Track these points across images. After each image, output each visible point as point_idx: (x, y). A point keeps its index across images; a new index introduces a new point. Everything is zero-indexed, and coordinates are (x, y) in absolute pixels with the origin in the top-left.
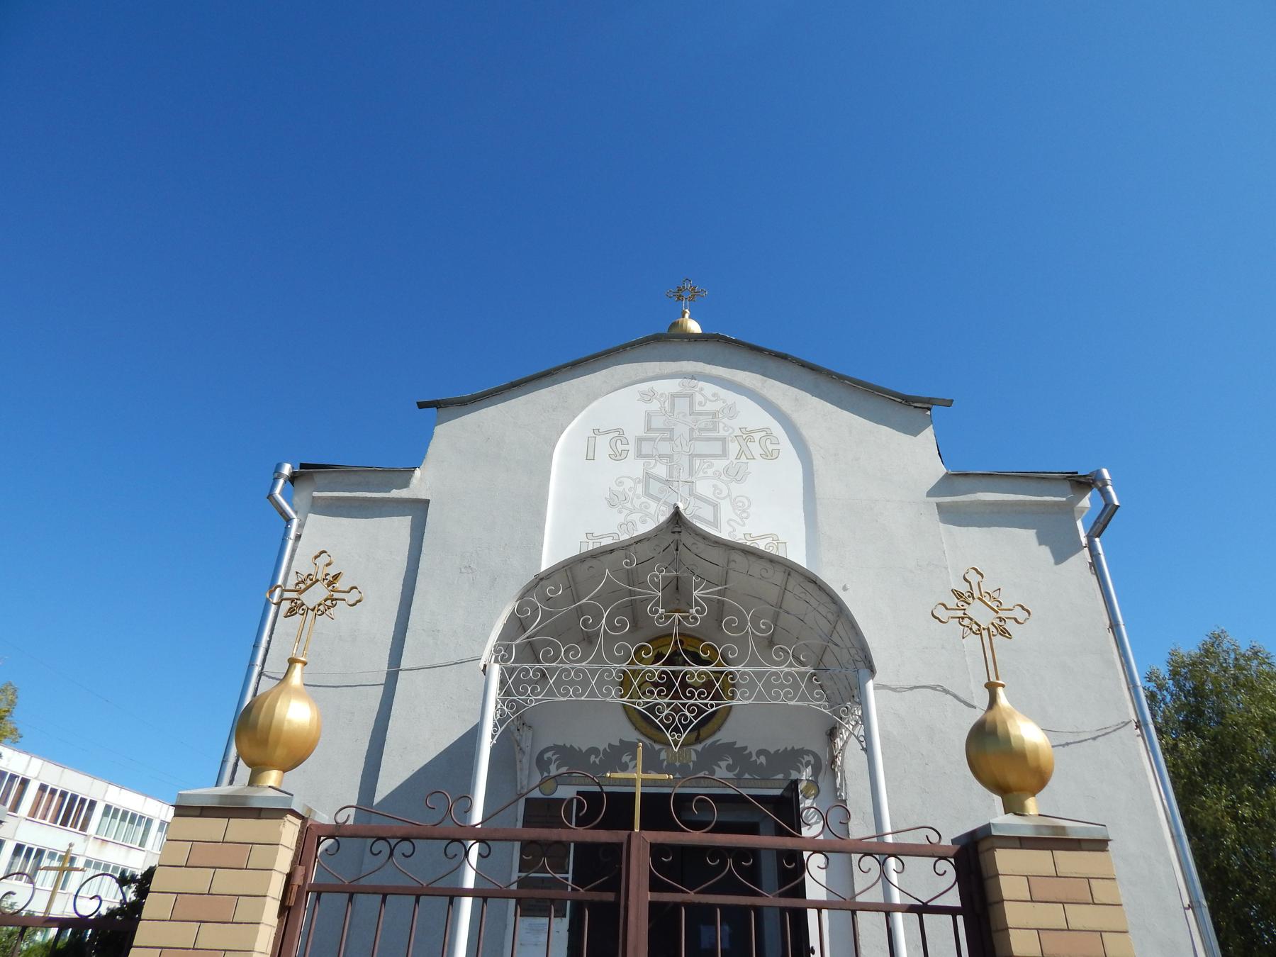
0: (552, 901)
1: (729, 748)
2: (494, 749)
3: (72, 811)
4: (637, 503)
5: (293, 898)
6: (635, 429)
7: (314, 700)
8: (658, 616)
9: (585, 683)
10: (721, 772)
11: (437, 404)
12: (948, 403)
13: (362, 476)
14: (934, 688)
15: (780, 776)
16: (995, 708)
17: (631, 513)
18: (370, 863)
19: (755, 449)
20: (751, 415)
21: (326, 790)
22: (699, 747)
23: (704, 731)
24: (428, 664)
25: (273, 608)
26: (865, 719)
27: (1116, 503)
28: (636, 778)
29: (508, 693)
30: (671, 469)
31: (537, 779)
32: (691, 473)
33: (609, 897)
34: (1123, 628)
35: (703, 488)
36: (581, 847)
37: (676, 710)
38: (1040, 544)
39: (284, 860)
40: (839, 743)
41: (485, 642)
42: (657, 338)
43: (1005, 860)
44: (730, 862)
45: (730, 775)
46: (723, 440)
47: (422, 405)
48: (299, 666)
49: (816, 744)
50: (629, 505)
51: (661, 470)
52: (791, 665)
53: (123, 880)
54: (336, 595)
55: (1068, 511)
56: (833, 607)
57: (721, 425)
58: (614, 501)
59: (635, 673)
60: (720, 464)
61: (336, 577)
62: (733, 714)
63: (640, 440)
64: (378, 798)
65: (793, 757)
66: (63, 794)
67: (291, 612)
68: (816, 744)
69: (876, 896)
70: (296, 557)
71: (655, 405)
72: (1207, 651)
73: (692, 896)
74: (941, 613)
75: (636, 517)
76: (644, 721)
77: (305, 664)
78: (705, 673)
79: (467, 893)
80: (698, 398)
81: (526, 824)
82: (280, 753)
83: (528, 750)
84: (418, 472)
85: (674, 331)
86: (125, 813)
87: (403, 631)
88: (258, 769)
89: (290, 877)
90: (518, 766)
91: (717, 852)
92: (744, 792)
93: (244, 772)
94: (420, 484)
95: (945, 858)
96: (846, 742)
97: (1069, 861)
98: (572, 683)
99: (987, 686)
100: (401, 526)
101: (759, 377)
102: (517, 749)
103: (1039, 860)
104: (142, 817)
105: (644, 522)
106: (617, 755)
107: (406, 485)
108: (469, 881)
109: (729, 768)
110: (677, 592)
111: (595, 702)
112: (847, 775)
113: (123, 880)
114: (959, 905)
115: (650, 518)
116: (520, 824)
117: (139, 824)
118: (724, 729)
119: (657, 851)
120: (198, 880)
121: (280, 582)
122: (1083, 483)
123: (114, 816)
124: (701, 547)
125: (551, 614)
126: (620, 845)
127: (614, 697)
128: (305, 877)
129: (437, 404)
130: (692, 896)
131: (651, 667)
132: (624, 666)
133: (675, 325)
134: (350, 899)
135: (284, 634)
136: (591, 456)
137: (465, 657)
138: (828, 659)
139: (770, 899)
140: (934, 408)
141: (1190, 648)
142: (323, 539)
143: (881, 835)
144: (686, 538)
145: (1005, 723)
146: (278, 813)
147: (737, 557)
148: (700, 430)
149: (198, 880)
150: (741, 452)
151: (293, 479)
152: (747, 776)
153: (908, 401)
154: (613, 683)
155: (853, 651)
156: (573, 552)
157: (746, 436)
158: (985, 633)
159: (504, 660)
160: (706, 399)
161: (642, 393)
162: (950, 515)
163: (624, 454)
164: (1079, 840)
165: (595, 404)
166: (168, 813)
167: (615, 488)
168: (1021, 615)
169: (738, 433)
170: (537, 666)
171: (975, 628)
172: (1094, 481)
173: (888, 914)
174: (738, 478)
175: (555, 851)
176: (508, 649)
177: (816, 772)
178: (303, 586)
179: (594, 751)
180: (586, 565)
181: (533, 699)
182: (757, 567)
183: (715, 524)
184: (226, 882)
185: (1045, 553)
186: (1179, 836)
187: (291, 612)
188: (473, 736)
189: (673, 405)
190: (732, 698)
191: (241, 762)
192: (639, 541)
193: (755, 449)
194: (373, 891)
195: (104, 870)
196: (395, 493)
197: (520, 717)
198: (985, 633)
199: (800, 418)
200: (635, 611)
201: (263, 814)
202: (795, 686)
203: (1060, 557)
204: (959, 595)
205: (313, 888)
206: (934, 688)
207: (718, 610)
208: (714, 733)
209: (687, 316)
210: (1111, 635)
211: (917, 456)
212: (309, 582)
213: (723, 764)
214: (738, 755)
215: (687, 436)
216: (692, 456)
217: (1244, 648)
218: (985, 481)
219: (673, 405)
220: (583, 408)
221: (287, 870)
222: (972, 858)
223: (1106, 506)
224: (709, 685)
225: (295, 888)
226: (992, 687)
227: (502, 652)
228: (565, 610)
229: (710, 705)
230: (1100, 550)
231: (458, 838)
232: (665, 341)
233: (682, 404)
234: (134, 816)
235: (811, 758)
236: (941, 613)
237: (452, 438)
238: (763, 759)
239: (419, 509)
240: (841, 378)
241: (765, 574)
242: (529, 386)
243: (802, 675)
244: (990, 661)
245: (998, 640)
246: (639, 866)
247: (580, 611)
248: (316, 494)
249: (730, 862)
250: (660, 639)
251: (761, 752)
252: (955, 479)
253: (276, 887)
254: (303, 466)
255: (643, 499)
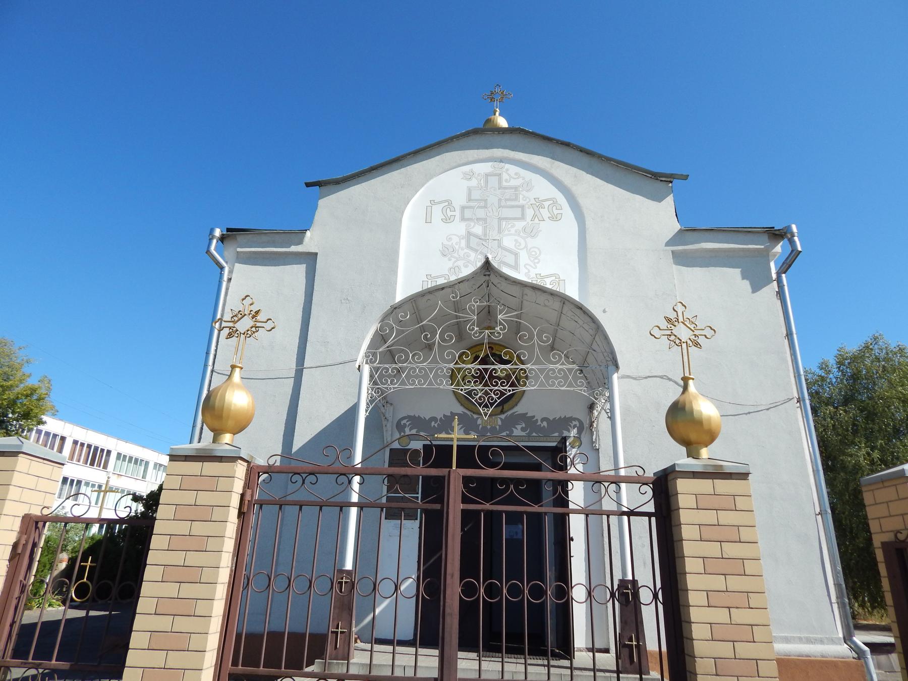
0: (403, 509)
1: (523, 417)
2: (367, 419)
3: (96, 457)
4: (461, 253)
5: (246, 507)
6: (460, 200)
7: (248, 389)
8: (475, 332)
9: (426, 377)
10: (517, 432)
11: (319, 184)
12: (685, 177)
13: (270, 237)
14: (661, 377)
15: (556, 434)
16: (687, 393)
17: (457, 260)
18: (291, 487)
19: (545, 213)
20: (543, 189)
21: (262, 445)
22: (503, 416)
23: (506, 406)
24: (323, 364)
25: (216, 332)
26: (610, 399)
27: (800, 249)
28: (456, 436)
29: (375, 383)
30: (485, 229)
31: (397, 435)
32: (500, 231)
33: (437, 506)
34: (795, 336)
35: (508, 242)
36: (426, 479)
37: (486, 393)
38: (743, 279)
39: (238, 486)
40: (596, 413)
41: (359, 349)
42: (476, 132)
43: (682, 485)
44: (512, 486)
45: (524, 434)
46: (522, 207)
47: (308, 185)
48: (238, 370)
49: (582, 415)
50: (456, 255)
51: (478, 230)
52: (563, 364)
53: (136, 498)
54: (258, 324)
55: (765, 256)
56: (593, 325)
57: (521, 196)
58: (447, 251)
59: (459, 370)
60: (520, 225)
61: (257, 312)
62: (526, 395)
63: (463, 208)
64: (295, 448)
65: (565, 422)
66: (89, 446)
67: (230, 336)
68: (582, 415)
69: (613, 507)
70: (229, 293)
71: (474, 182)
72: (867, 347)
73: (488, 506)
74: (656, 332)
75: (460, 263)
76: (465, 400)
77: (242, 368)
78: (505, 369)
79: (354, 505)
80: (505, 176)
81: (391, 464)
82: (230, 423)
83: (390, 419)
84: (308, 233)
85: (488, 126)
86: (131, 458)
87: (302, 342)
88: (217, 433)
89: (243, 496)
90: (385, 429)
91: (505, 481)
92: (520, 444)
93: (208, 435)
94: (311, 242)
95: (646, 484)
96: (600, 413)
97: (722, 485)
98: (417, 377)
99: (682, 379)
100: (299, 271)
101: (549, 160)
102: (383, 418)
103: (705, 485)
104: (142, 461)
105: (466, 266)
106: (446, 424)
107: (300, 242)
108: (355, 498)
109: (523, 429)
110: (488, 316)
111: (434, 390)
112: (600, 433)
113: (136, 498)
114: (653, 511)
115: (469, 266)
116: (386, 465)
117: (140, 465)
118: (520, 405)
119: (466, 480)
120: (188, 497)
121: (219, 316)
122: (777, 235)
123: (124, 460)
124: (504, 285)
125: (403, 332)
126: (444, 477)
127: (446, 385)
128: (252, 496)
129: (319, 184)
130: (488, 506)
131: (469, 366)
132: (452, 365)
133: (488, 121)
134: (280, 508)
135: (225, 350)
136: (429, 220)
137: (347, 359)
138: (590, 359)
139: (547, 508)
140: (675, 181)
141: (853, 347)
142: (248, 284)
143: (617, 469)
144: (493, 278)
145: (691, 402)
146: (233, 459)
147: (528, 291)
148: (506, 200)
149: (188, 497)
150: (535, 216)
151: (222, 239)
152: (534, 434)
153: (656, 176)
154: (444, 376)
155: (605, 354)
156: (417, 289)
157: (539, 204)
158: (684, 345)
159: (372, 362)
160: (511, 177)
161: (465, 174)
162: (681, 259)
163: (452, 219)
164: (731, 473)
165: (431, 182)
166: (165, 460)
167: (446, 243)
168: (708, 333)
169: (533, 202)
170: (394, 366)
171: (678, 341)
172: (785, 233)
173: (587, 515)
174: (532, 234)
175: (408, 483)
176: (374, 354)
177: (580, 431)
178: (236, 319)
179: (434, 419)
180: (426, 298)
181: (392, 387)
182: (542, 298)
183: (516, 267)
184: (205, 498)
185: (746, 285)
186: (818, 470)
187: (230, 336)
188: (353, 411)
189: (487, 182)
190: (525, 385)
191: (205, 427)
192: (461, 281)
193: (545, 213)
194: (294, 503)
195: (125, 493)
196: (293, 249)
197: (385, 398)
198: (684, 345)
199: (577, 190)
200: (460, 331)
201: (733, 476)
202: (565, 377)
203: (755, 288)
204: (669, 320)
205: (257, 502)
206: (661, 377)
207: (516, 328)
208: (513, 407)
209: (497, 114)
210: (786, 341)
211: (660, 216)
212: (240, 316)
213: (519, 427)
214: (529, 421)
215: (497, 205)
216: (500, 219)
217: (893, 346)
218: (707, 234)
219: (487, 182)
220: (423, 185)
221: (241, 492)
222: (663, 485)
223: (792, 251)
224: (508, 377)
225: (246, 502)
226: (685, 380)
227: (371, 356)
228: (412, 328)
229: (508, 390)
230: (785, 282)
231: (347, 473)
232: (481, 133)
233: (493, 181)
234: (136, 460)
235: (577, 423)
236: (656, 332)
237: (331, 207)
238: (545, 424)
239: (310, 259)
240: (608, 160)
241: (546, 302)
242: (384, 169)
243: (570, 370)
244: (686, 363)
245: (693, 349)
246: (455, 489)
247: (423, 329)
248: (239, 250)
249: (512, 486)
250: (475, 347)
251: (543, 420)
252: (687, 232)
253: (235, 501)
254: (228, 230)
255: (466, 251)
